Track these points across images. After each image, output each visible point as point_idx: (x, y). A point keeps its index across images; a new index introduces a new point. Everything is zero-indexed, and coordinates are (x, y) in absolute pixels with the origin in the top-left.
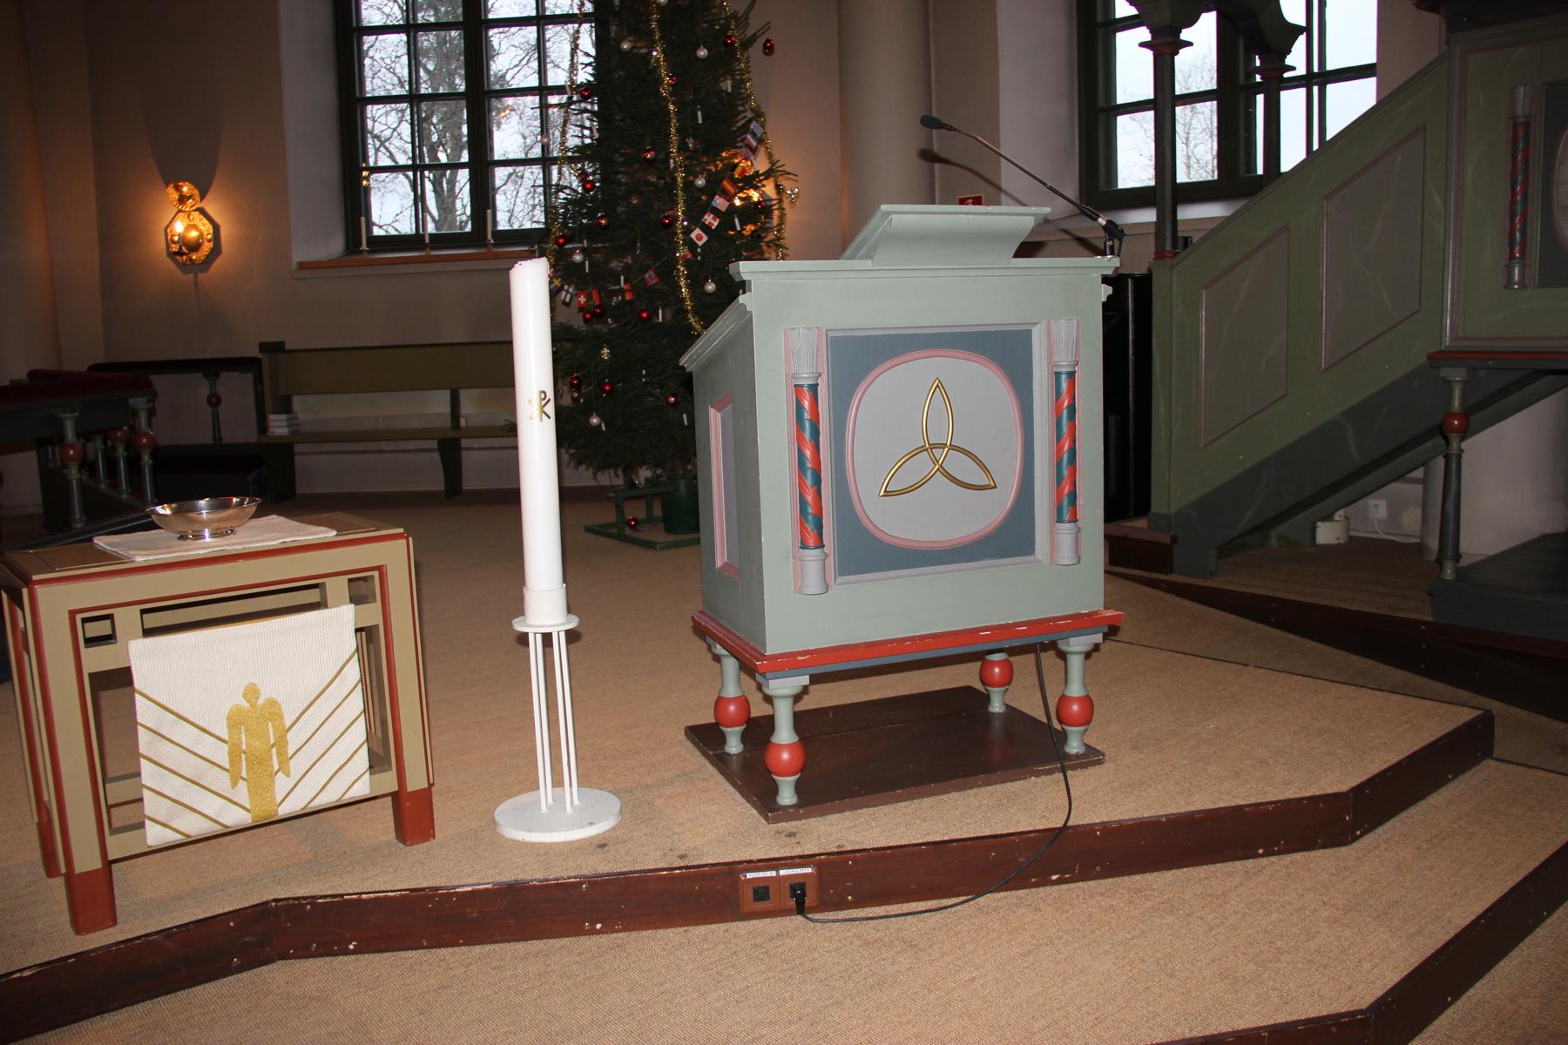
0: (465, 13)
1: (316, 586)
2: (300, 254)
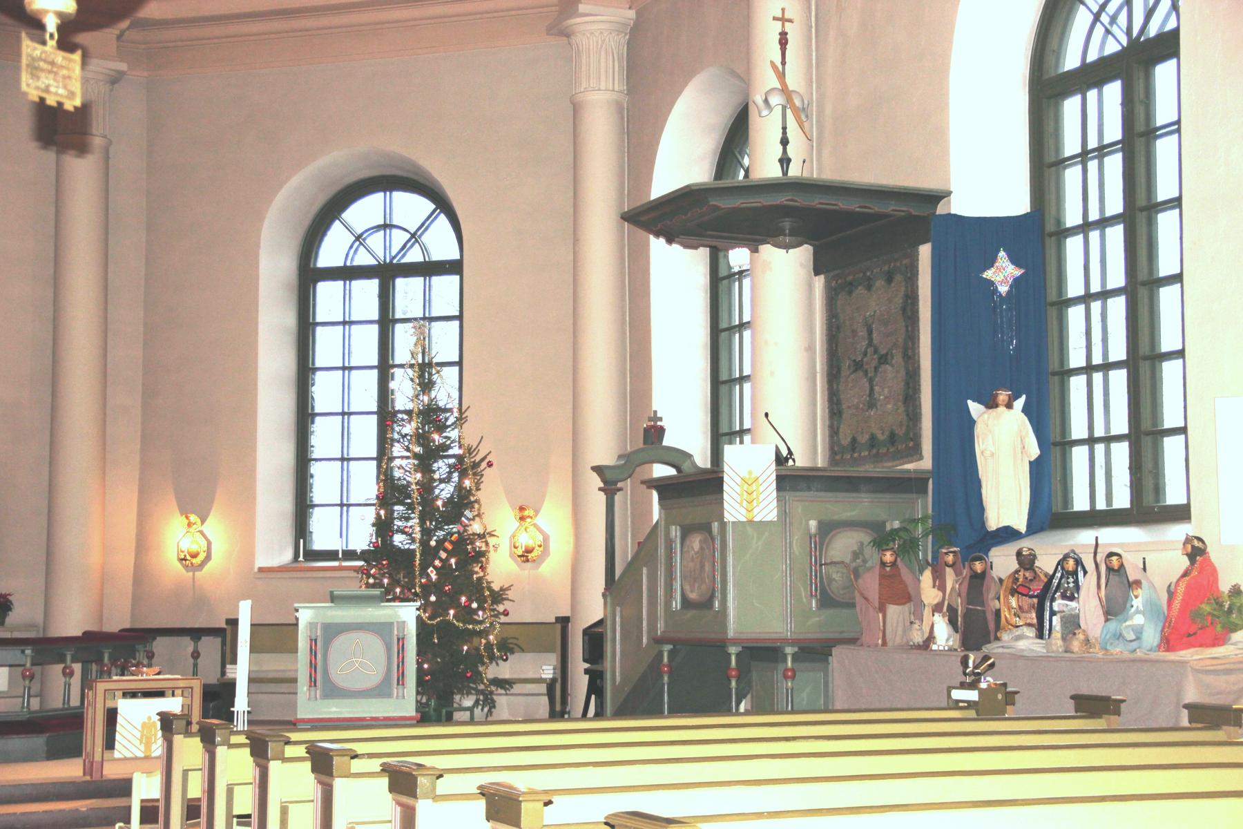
0: (379, 407)
1: (284, 811)
2: (262, 561)
